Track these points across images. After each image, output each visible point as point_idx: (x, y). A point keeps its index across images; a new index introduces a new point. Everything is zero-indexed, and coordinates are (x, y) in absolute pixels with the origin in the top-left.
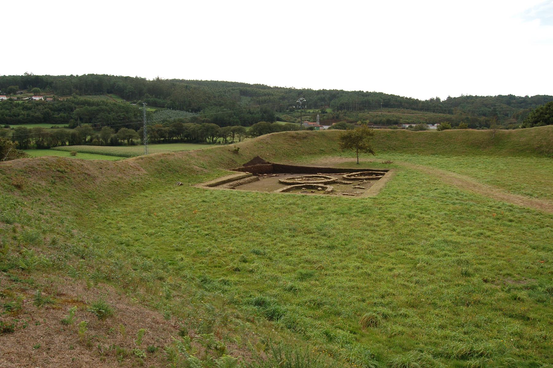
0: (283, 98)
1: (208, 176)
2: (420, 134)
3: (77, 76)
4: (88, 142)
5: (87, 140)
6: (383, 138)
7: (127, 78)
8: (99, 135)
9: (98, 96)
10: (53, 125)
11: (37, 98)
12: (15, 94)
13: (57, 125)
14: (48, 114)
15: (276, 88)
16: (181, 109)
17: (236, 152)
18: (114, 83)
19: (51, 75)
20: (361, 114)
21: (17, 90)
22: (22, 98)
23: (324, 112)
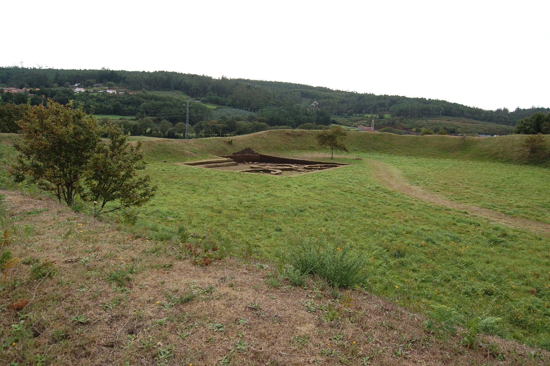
0: (343, 102)
1: (193, 158)
2: (403, 137)
3: (149, 72)
4: (148, 133)
5: (147, 131)
6: (370, 140)
7: (195, 76)
8: (159, 128)
9: (166, 92)
10: (122, 117)
11: (111, 92)
12: (92, 87)
13: (125, 117)
14: (118, 106)
15: (338, 91)
16: (241, 107)
17: (230, 143)
18: (182, 81)
19: (126, 70)
20: (417, 122)
21: (94, 84)
22: (98, 90)
23: (381, 117)
